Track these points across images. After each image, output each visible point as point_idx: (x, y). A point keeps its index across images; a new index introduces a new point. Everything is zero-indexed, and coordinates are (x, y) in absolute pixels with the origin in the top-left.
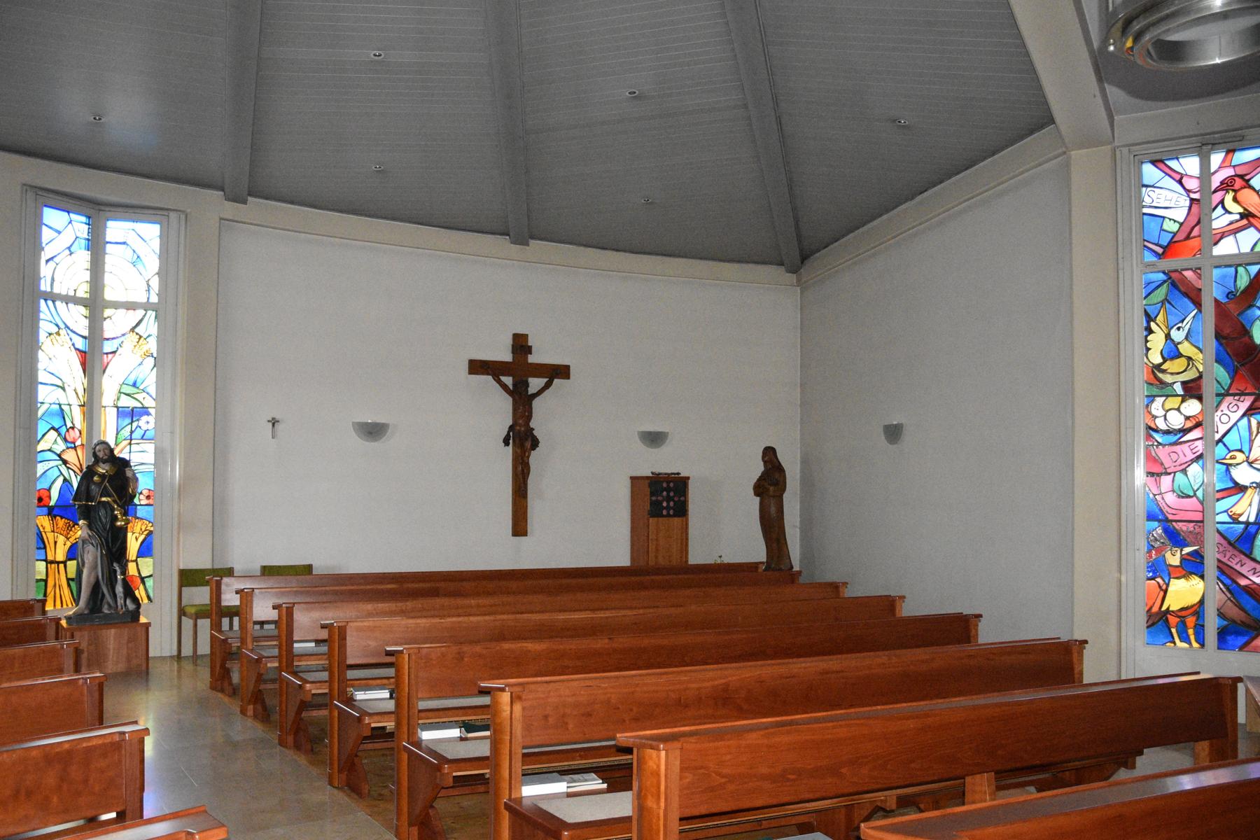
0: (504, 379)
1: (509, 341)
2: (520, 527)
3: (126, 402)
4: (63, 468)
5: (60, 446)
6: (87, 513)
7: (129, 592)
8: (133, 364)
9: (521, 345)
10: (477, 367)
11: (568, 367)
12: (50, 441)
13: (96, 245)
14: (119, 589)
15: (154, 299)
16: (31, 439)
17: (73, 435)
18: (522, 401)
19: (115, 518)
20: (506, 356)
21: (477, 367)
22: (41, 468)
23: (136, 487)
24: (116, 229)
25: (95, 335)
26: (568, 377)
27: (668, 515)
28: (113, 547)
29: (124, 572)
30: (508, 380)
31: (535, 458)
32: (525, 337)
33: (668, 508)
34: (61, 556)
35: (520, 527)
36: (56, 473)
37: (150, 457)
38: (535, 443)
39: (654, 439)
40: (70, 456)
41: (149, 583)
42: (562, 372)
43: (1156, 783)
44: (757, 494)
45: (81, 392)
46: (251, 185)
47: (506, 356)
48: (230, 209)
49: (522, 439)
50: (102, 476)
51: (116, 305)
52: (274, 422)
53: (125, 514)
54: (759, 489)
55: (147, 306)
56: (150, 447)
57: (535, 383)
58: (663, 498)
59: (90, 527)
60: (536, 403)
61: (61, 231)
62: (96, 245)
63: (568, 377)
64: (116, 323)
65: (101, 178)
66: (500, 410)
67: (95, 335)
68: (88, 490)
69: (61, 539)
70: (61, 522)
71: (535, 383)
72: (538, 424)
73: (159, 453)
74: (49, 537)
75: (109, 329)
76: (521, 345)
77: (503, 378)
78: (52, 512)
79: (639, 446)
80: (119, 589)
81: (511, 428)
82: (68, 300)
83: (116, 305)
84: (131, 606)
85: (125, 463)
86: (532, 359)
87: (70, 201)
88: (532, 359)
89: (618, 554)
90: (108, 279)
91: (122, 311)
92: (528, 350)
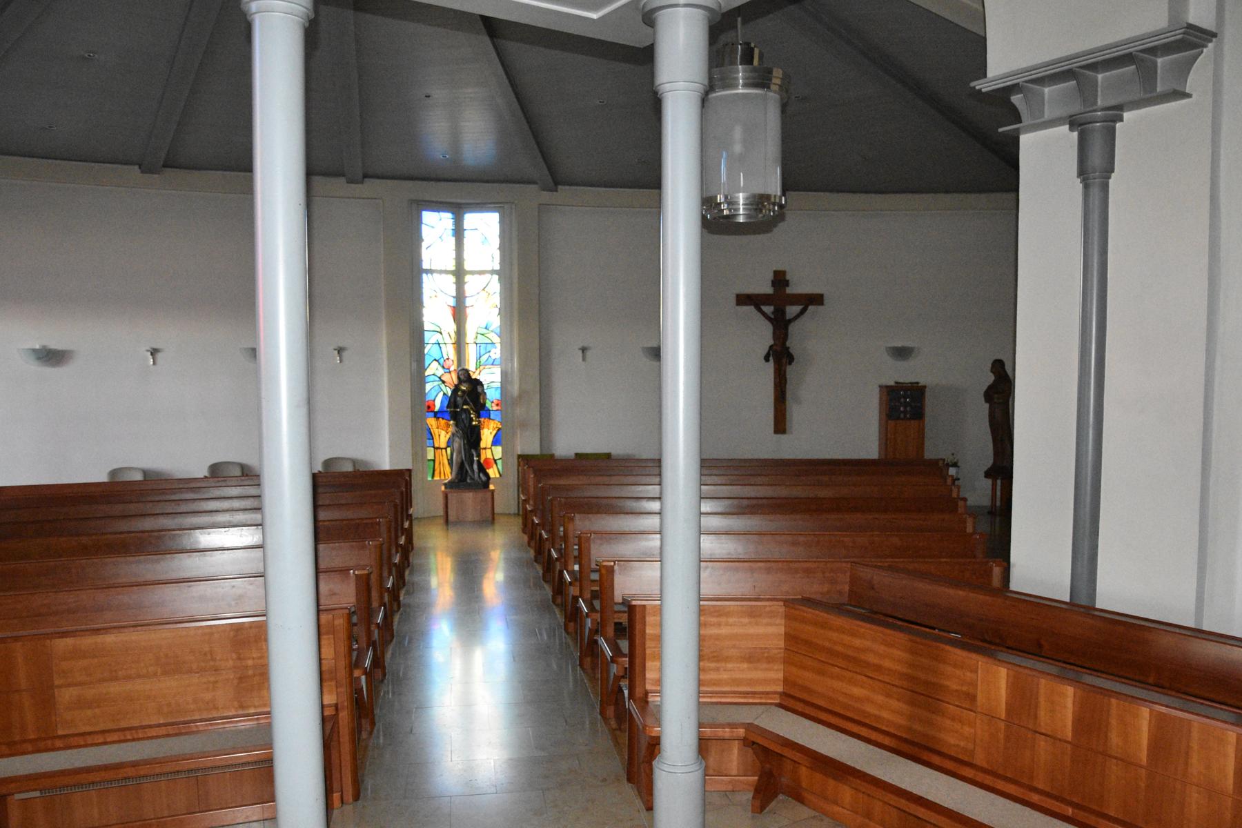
0: (765, 308)
1: (770, 276)
2: (780, 425)
3: (481, 339)
4: (443, 386)
5: (440, 372)
6: (455, 416)
7: (482, 469)
8: (486, 306)
9: (780, 280)
10: (743, 299)
11: (822, 296)
12: (433, 369)
13: (459, 232)
14: (475, 467)
15: (497, 267)
16: (421, 367)
17: (448, 363)
18: (781, 325)
19: (471, 420)
20: (769, 290)
21: (743, 299)
22: (428, 387)
23: (485, 399)
24: (470, 219)
25: (460, 297)
26: (822, 304)
27: (905, 419)
28: (471, 438)
29: (479, 456)
30: (768, 309)
31: (791, 371)
32: (783, 273)
33: (905, 412)
34: (443, 445)
35: (780, 425)
36: (437, 392)
37: (497, 377)
38: (791, 359)
39: (902, 353)
40: (446, 378)
41: (499, 462)
42: (817, 299)
43: (715, 510)
44: (986, 401)
45: (453, 335)
46: (556, 179)
47: (769, 290)
48: (546, 196)
49: (781, 356)
50: (463, 392)
51: (472, 273)
52: (584, 350)
53: (479, 416)
54: (989, 395)
55: (493, 272)
56: (497, 371)
57: (792, 310)
58: (903, 404)
59: (457, 425)
60: (794, 329)
61: (435, 227)
62: (459, 232)
63: (822, 304)
64: (472, 284)
65: (458, 188)
66: (764, 335)
67: (460, 297)
68: (455, 401)
69: (443, 433)
70: (442, 422)
71: (792, 310)
72: (793, 344)
73: (504, 375)
74: (435, 431)
75: (469, 290)
76: (780, 280)
77: (763, 308)
78: (437, 415)
79: (889, 361)
80: (475, 467)
81: (771, 347)
82: (441, 272)
83: (472, 273)
84: (484, 478)
85: (478, 383)
86: (789, 291)
87: (438, 206)
88: (789, 291)
89: (869, 449)
90: (466, 255)
91: (477, 276)
92: (787, 283)
